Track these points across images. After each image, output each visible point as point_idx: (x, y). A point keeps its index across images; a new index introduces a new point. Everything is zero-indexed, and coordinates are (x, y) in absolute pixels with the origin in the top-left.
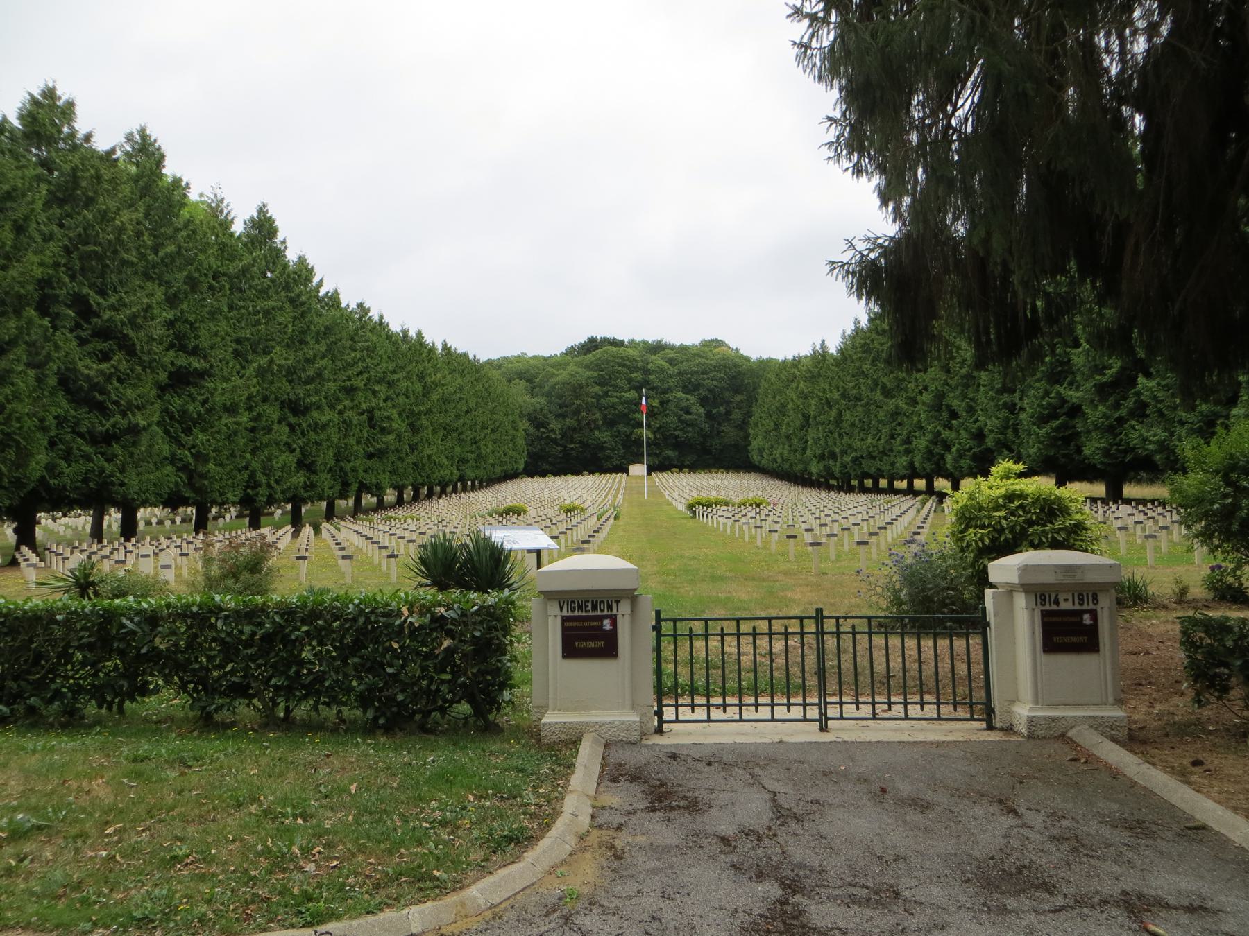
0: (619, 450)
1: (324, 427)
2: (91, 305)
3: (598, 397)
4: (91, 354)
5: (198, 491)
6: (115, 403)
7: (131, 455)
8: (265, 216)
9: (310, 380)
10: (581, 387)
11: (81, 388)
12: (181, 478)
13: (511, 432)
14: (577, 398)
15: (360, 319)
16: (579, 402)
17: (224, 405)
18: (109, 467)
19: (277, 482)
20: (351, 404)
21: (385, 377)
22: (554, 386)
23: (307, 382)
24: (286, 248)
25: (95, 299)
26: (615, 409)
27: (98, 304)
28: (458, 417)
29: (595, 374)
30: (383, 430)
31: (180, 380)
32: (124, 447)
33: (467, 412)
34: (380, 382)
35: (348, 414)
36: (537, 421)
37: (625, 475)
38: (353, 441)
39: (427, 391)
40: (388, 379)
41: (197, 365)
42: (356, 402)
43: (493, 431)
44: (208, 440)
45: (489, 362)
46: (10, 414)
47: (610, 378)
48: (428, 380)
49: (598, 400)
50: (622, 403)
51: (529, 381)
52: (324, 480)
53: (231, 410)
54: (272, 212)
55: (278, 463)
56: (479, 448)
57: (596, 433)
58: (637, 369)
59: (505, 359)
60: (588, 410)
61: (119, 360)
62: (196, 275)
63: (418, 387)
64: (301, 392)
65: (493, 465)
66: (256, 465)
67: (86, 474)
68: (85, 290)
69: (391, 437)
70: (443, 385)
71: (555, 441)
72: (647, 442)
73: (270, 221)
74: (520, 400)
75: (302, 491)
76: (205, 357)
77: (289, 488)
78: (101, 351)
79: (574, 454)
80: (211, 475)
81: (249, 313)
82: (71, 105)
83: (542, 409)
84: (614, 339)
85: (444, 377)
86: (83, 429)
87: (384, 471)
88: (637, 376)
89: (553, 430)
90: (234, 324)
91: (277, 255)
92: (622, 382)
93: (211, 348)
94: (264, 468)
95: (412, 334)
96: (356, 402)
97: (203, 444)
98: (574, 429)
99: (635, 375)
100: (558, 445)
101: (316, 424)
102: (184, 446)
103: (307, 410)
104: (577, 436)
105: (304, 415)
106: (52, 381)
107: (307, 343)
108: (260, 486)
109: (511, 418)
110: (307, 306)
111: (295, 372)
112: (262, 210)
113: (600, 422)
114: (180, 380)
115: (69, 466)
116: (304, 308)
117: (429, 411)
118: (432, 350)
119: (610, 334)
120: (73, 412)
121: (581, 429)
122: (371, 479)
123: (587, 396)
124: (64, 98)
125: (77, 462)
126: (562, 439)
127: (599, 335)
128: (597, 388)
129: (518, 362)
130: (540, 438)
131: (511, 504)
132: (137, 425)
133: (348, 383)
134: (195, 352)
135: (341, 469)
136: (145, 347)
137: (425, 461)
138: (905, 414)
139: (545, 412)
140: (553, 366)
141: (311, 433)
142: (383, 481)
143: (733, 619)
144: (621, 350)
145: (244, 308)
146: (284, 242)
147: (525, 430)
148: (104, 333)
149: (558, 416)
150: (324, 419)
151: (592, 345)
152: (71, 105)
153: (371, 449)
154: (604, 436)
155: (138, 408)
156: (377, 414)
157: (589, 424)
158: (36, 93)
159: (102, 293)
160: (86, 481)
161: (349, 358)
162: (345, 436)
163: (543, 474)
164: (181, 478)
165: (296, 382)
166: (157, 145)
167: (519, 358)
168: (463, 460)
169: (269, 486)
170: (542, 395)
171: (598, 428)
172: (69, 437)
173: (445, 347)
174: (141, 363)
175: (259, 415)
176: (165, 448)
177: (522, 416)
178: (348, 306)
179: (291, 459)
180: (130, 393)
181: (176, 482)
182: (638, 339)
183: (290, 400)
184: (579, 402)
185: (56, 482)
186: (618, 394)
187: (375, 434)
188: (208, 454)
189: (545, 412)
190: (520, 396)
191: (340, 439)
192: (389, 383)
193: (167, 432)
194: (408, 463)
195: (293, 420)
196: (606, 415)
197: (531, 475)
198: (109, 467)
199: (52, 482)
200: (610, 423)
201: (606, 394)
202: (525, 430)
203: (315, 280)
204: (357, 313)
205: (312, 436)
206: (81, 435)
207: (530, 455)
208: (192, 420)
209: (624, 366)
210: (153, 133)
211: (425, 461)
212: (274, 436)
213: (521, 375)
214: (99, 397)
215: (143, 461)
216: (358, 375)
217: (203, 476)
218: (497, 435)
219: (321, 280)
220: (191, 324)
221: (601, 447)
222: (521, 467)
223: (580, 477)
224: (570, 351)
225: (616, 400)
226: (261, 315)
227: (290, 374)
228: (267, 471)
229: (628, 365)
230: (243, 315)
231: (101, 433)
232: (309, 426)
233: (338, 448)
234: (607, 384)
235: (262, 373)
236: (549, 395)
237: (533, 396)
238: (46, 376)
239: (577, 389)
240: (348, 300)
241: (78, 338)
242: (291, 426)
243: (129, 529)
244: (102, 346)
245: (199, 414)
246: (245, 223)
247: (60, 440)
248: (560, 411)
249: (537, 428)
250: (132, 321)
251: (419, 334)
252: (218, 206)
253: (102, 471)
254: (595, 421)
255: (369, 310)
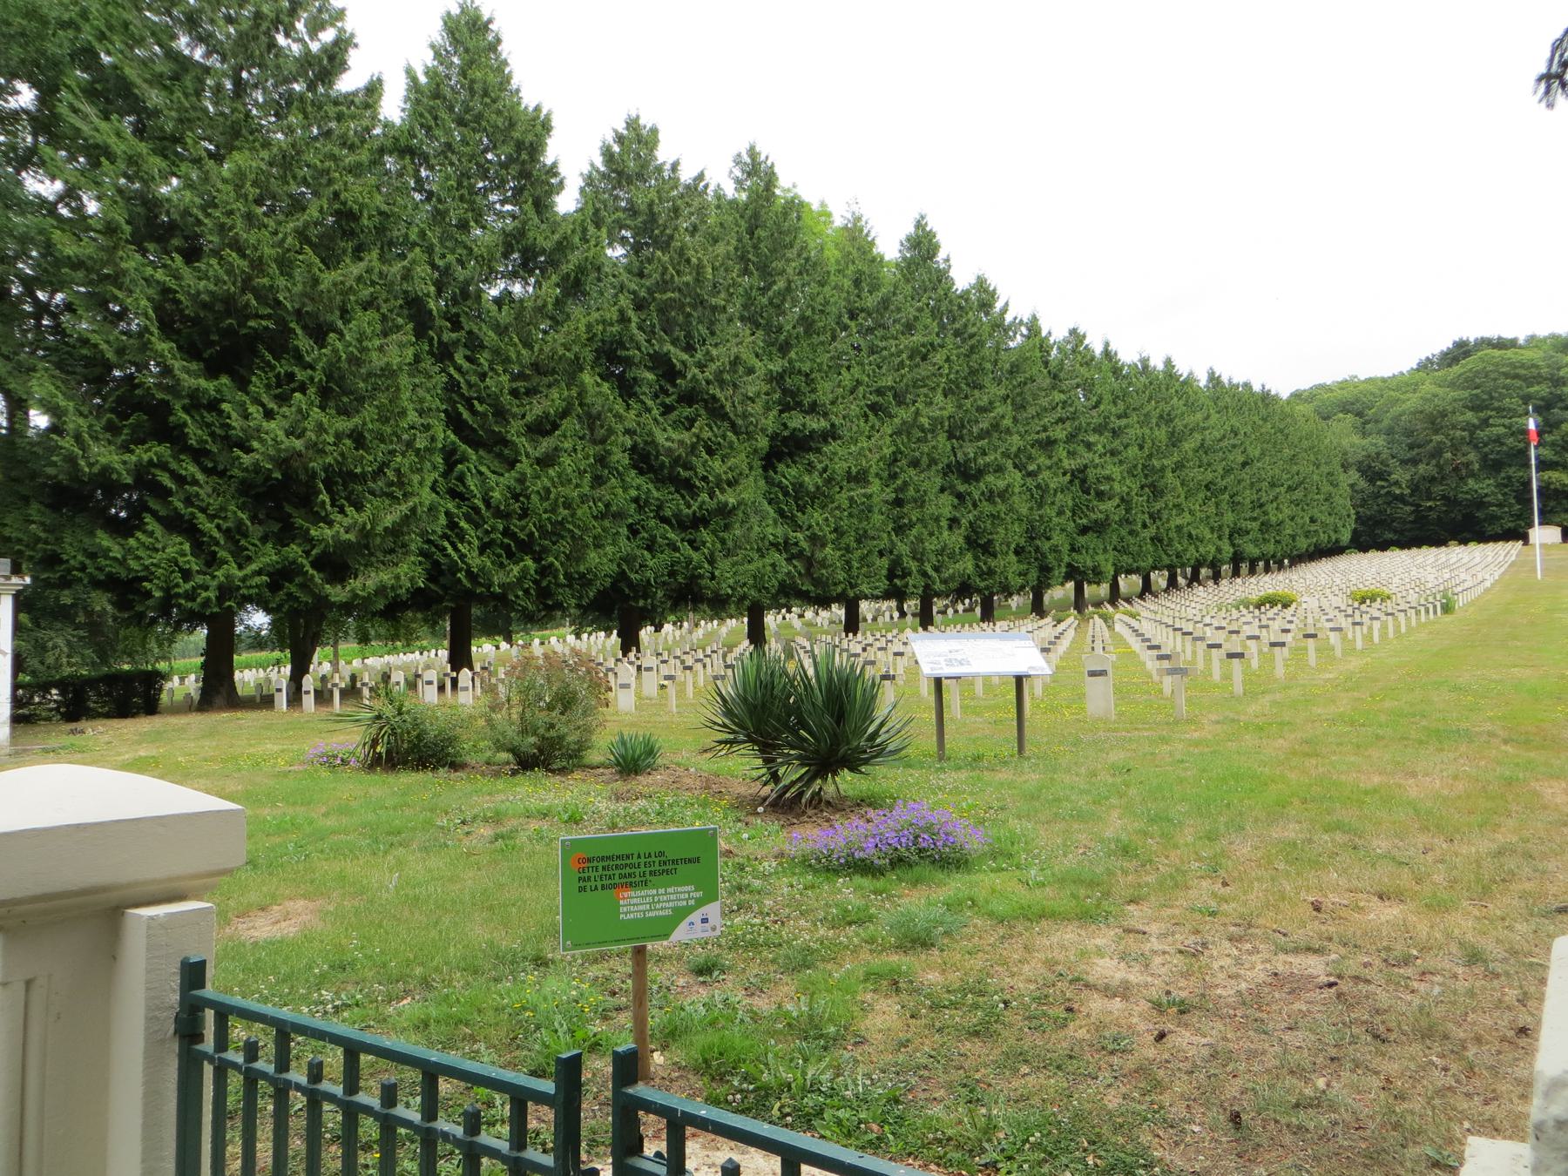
0: (1511, 505)
1: (1004, 494)
2: (674, 366)
3: (1471, 428)
4: (676, 425)
5: (817, 582)
6: (704, 479)
7: (723, 542)
8: (924, 230)
9: (984, 434)
10: (1443, 414)
11: (662, 465)
12: (795, 567)
13: (1326, 488)
14: (1436, 432)
15: (1074, 351)
16: (1438, 438)
17: (849, 472)
18: (695, 556)
19: (937, 569)
20: (1048, 462)
21: (1107, 424)
22: (1397, 418)
23: (980, 437)
24: (950, 266)
25: (678, 355)
26: (1503, 444)
27: (684, 363)
28: (1228, 471)
29: (1465, 394)
30: (1100, 495)
31: (787, 447)
32: (714, 532)
33: (1244, 464)
34: (1098, 430)
35: (1045, 475)
36: (1372, 471)
37: (1521, 542)
38: (1050, 511)
39: (1175, 440)
40: (1112, 426)
41: (815, 426)
42: (1055, 459)
43: (1290, 489)
44: (826, 519)
45: (1297, 396)
46: (556, 500)
47: (1492, 398)
48: (1178, 424)
49: (1472, 434)
50: (1513, 434)
51: (1359, 414)
52: (1008, 565)
53: (860, 478)
54: (932, 224)
55: (931, 545)
56: (1266, 513)
57: (1471, 482)
58: (1539, 379)
59: (1322, 387)
60: (1455, 448)
61: (704, 429)
62: (809, 313)
63: (1162, 434)
64: (970, 450)
65: (1293, 537)
66: (903, 548)
67: (672, 566)
68: (668, 347)
69: (1108, 506)
70: (1204, 429)
71: (1401, 499)
72: (1538, 491)
73: (930, 236)
74: (1345, 442)
75: (978, 580)
76: (825, 415)
77: (952, 577)
78: (687, 418)
79: (1433, 515)
80: (830, 562)
81: (892, 355)
82: (654, 131)
83: (1378, 454)
84: (1499, 338)
85: (1207, 418)
86: (668, 513)
87: (1105, 551)
88: (1542, 390)
89: (1397, 483)
90: (874, 372)
91: (941, 278)
92: (1512, 402)
93: (833, 403)
94: (914, 551)
95: (1157, 363)
96: (1055, 459)
97: (818, 524)
98: (1432, 480)
99: (1536, 388)
100: (1405, 503)
101: (991, 492)
102: (801, 527)
103: (979, 474)
104: (1438, 489)
105: (978, 480)
106: (620, 458)
107: (981, 387)
108: (910, 574)
109: (1325, 469)
110: (977, 338)
111: (963, 426)
112: (919, 225)
113: (1476, 466)
114: (787, 447)
115: (654, 557)
116: (973, 341)
117: (1179, 466)
118: (1189, 382)
119: (1492, 332)
120: (656, 494)
121: (1443, 478)
122: (1084, 561)
123: (1454, 427)
124: (649, 126)
125: (662, 552)
126: (1411, 495)
127: (1472, 334)
128: (1469, 415)
129: (1341, 389)
130: (1376, 496)
131: (1270, 591)
132: (726, 504)
133: (1044, 435)
134: (813, 409)
135: (1037, 549)
136: (740, 409)
137: (1173, 534)
138: (309, 272)
139: (1384, 456)
140: (1398, 389)
141: (985, 503)
142: (1103, 563)
143: (336, 1039)
144: (1509, 353)
145: (885, 348)
146: (947, 260)
147: (1352, 486)
148: (689, 398)
149: (1404, 462)
150: (1001, 484)
151: (1461, 351)
152: (654, 131)
153: (1084, 521)
154: (1484, 486)
155: (730, 484)
156: (1091, 474)
157: (1456, 469)
158: (621, 128)
159: (690, 348)
160: (672, 574)
161: (1044, 402)
162: (1040, 506)
163: (1383, 546)
164: (795, 567)
165: (967, 438)
166: (769, 163)
167: (1343, 385)
168: (1236, 532)
169: (924, 574)
170: (1379, 433)
171: (1473, 475)
172: (652, 523)
173: (1214, 379)
174: (734, 427)
175: (905, 484)
176: (777, 531)
177: (1345, 467)
178: (1050, 333)
179: (955, 539)
180: (716, 464)
181: (789, 573)
182: (1543, 332)
183: (957, 462)
184: (1438, 438)
185: (638, 577)
186: (1507, 421)
187: (1090, 501)
188: (825, 536)
189: (1384, 456)
190: (1345, 437)
191: (1031, 509)
192: (1114, 431)
193: (781, 513)
194: (1144, 539)
195: (962, 488)
196: (1486, 455)
197: (1364, 549)
198: (695, 556)
199: (632, 576)
200: (1493, 466)
201: (1485, 423)
202: (1352, 486)
203: (999, 305)
204: (1069, 342)
205: (986, 507)
206: (665, 520)
207: (1359, 518)
208: (808, 493)
209: (1517, 376)
210: (763, 150)
211: (1173, 534)
212: (931, 509)
213: (1346, 407)
214: (684, 474)
215: (741, 548)
216: (1057, 423)
217: (823, 564)
218: (1298, 494)
219: (1007, 304)
220: (807, 375)
221: (1480, 503)
222: (1346, 537)
223: (1443, 549)
224: (1425, 366)
225: (1502, 430)
226: (904, 356)
227: (955, 432)
228: (918, 556)
229: (1523, 374)
230: (884, 359)
231: (687, 516)
232: (983, 493)
233: (1030, 522)
234: (1487, 408)
235: (904, 430)
236: (1390, 432)
237: (1364, 435)
238: (609, 453)
239: (1436, 420)
240: (1056, 329)
241: (663, 405)
242: (960, 497)
243: (852, 624)
244: (688, 411)
245: (818, 488)
246: (902, 245)
247: (643, 527)
248: (1410, 455)
249: (1372, 481)
250: (719, 375)
251: (1168, 363)
252: (855, 225)
253: (689, 561)
254: (1467, 465)
255: (1084, 336)
